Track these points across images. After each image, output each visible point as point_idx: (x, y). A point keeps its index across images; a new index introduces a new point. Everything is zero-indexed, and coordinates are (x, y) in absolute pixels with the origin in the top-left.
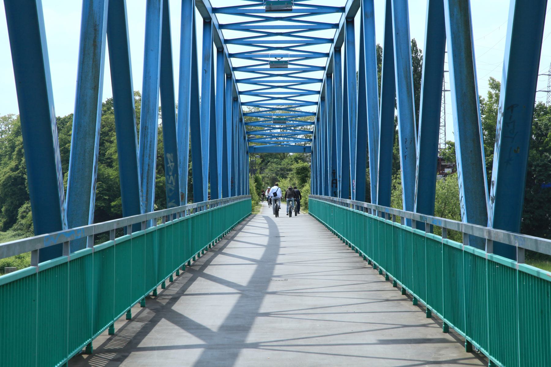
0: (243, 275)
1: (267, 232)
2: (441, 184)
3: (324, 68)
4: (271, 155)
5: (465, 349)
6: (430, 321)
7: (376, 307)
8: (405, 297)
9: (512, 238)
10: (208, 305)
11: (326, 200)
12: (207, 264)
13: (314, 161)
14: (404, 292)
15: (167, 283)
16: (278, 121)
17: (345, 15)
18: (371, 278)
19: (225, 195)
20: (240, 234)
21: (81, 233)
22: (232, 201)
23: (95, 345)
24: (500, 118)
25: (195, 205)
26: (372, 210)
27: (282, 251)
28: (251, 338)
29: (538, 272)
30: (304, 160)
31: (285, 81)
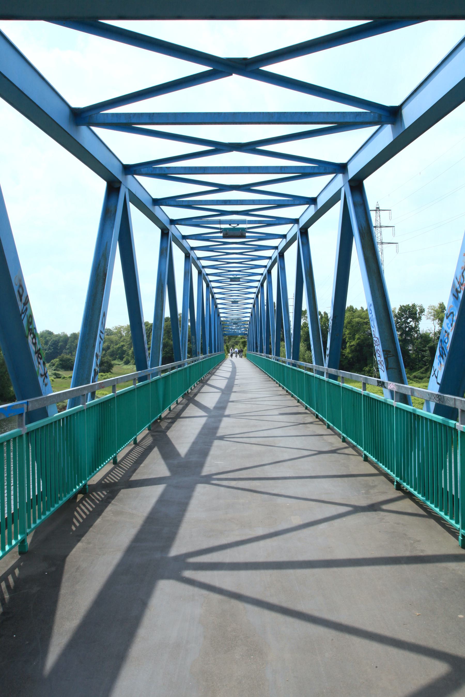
0: (222, 384)
1: (231, 366)
2: (282, 343)
3: (252, 303)
4: (232, 336)
5: (315, 417)
6: (299, 404)
7: (277, 398)
8: (287, 393)
9: (339, 373)
10: (209, 398)
11: (253, 353)
12: (208, 379)
13: (248, 339)
14: (287, 391)
15: (193, 388)
16: (235, 323)
17: (260, 283)
18: (273, 385)
19: (215, 352)
20: (221, 367)
21: (157, 370)
22: (217, 354)
23: (163, 416)
24: (331, 321)
25: (203, 356)
26: (272, 358)
27: (237, 374)
28: (227, 412)
29: (352, 388)
30: (244, 338)
31: (237, 308)
